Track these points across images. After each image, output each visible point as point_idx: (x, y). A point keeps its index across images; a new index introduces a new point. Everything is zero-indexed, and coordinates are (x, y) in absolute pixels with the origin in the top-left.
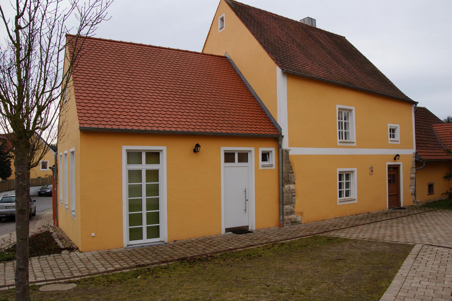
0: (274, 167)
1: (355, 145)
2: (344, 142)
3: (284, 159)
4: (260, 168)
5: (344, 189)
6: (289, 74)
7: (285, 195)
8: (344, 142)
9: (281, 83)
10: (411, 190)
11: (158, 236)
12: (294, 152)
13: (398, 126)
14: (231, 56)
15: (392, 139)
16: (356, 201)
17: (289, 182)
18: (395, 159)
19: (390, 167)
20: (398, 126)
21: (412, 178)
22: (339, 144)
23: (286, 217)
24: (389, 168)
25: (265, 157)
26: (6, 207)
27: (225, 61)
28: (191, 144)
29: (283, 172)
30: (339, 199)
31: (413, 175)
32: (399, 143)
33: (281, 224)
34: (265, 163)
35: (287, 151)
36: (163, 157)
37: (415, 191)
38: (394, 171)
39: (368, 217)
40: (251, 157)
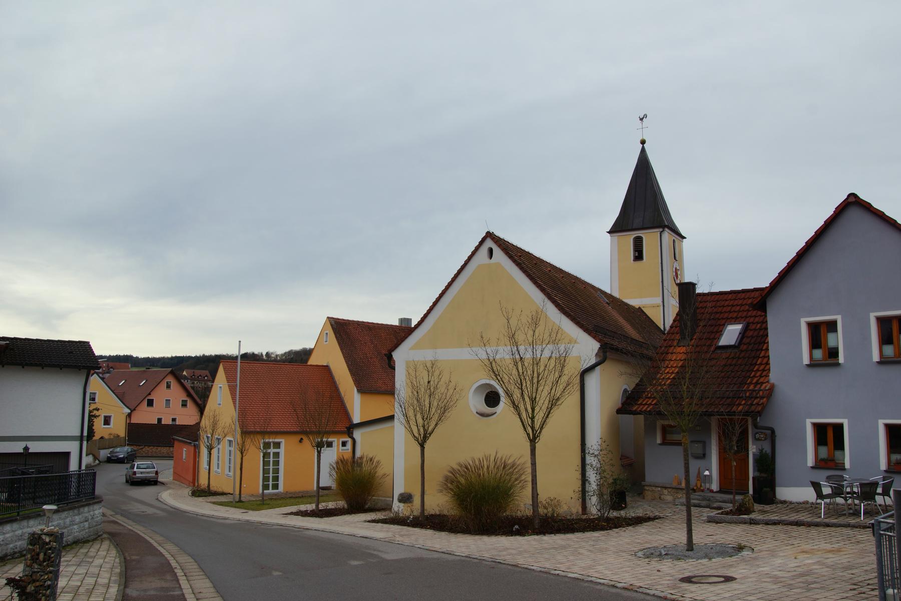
25: (344, 444)
26: (148, 473)
28: (298, 437)
36: (282, 446)
40: (335, 444)
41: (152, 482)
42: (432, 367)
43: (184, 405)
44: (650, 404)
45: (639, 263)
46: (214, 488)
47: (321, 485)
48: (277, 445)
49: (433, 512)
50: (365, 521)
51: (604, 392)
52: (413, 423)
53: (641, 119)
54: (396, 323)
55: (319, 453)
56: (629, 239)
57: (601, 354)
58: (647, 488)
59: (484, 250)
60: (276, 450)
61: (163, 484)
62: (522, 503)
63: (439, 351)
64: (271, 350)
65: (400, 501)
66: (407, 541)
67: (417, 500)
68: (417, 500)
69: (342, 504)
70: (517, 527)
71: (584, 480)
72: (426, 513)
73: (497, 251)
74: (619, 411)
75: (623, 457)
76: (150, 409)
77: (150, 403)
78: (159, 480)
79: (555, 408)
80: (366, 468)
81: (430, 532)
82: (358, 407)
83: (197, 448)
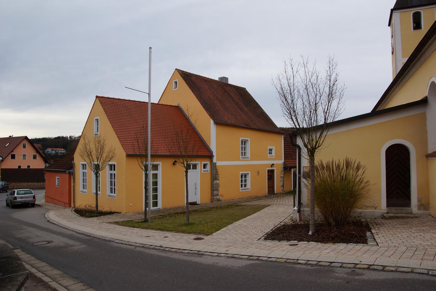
0: (209, 172)
1: (249, 159)
2: (244, 158)
4: (203, 172)
5: (244, 183)
6: (217, 123)
7: (214, 186)
8: (244, 158)
10: (281, 184)
11: (157, 206)
12: (219, 163)
13: (274, 147)
14: (183, 107)
15: (270, 155)
16: (250, 190)
17: (216, 179)
18: (272, 166)
19: (269, 171)
20: (274, 147)
21: (281, 177)
22: (241, 159)
23: (215, 197)
24: (268, 172)
25: (205, 166)
26: (27, 197)
27: (178, 108)
28: (173, 160)
30: (241, 188)
31: (282, 175)
32: (274, 157)
33: (212, 201)
34: (205, 170)
35: (215, 164)
36: (160, 168)
37: (283, 185)
38: (271, 173)
39: (256, 198)
40: (198, 167)
41: (29, 205)
43: (35, 157)
46: (103, 207)
47: (190, 201)
48: (155, 167)
54: (217, 79)
55: (187, 172)
60: (155, 172)
61: (39, 206)
64: (72, 135)
76: (13, 160)
77: (13, 157)
78: (36, 203)
83: (72, 175)
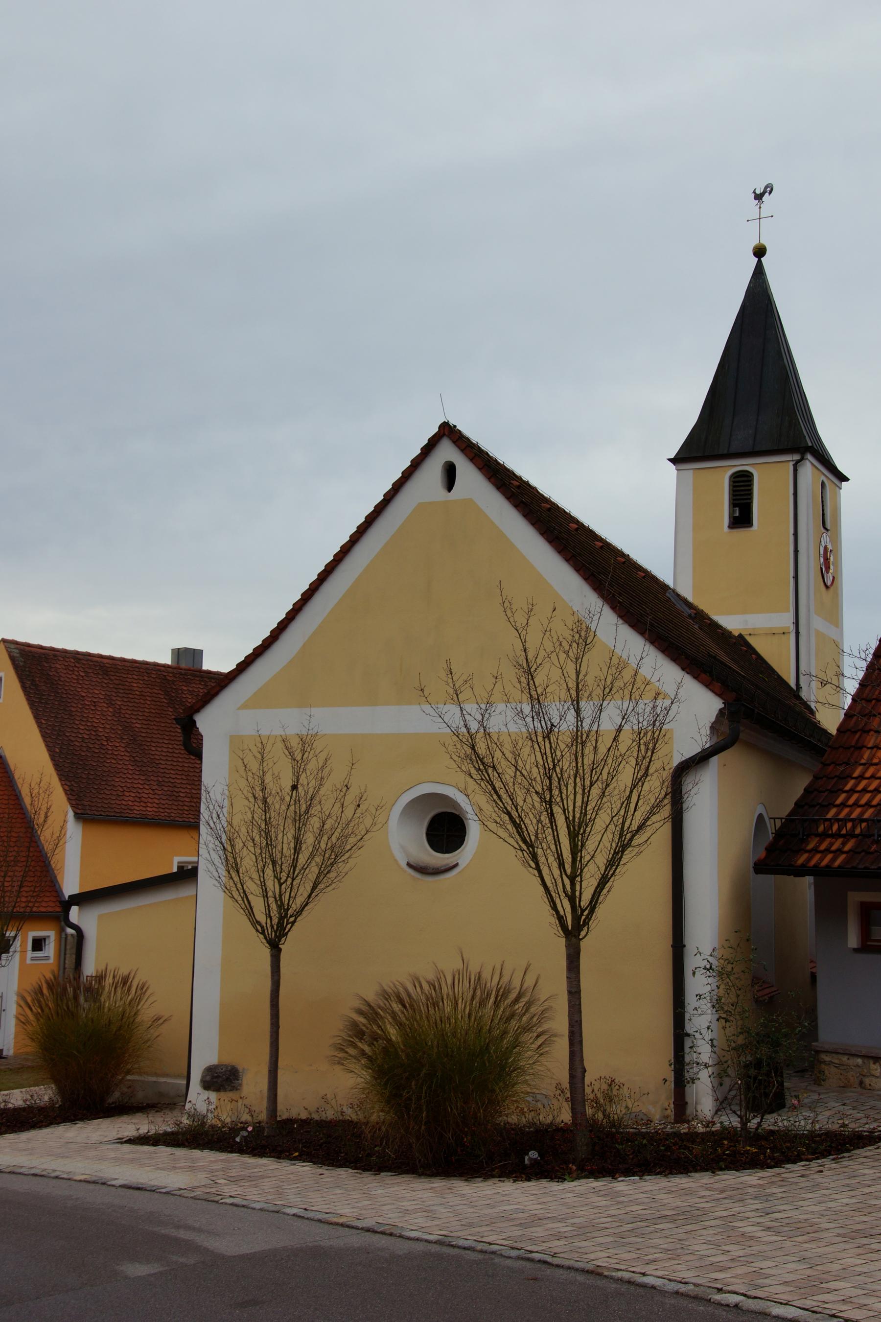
0: (51, 961)
3: (68, 947)
4: (29, 961)
9: (74, 831)
25: (38, 944)
29: (65, 968)
42: (300, 751)
44: (839, 851)
45: (741, 534)
49: (294, 1114)
50: (122, 1141)
51: (719, 820)
52: (252, 887)
53: (759, 197)
56: (719, 476)
57: (725, 728)
58: (826, 1058)
59: (433, 469)
62: (541, 1090)
63: (317, 712)
65: (207, 1085)
66: (255, 1196)
67: (254, 1085)
68: (254, 1085)
69: (45, 1094)
70: (534, 1154)
71: (680, 1035)
72: (283, 1113)
73: (466, 471)
74: (760, 867)
75: (755, 980)
79: (628, 854)
80: (111, 1000)
81: (305, 1169)
82: (75, 856)
